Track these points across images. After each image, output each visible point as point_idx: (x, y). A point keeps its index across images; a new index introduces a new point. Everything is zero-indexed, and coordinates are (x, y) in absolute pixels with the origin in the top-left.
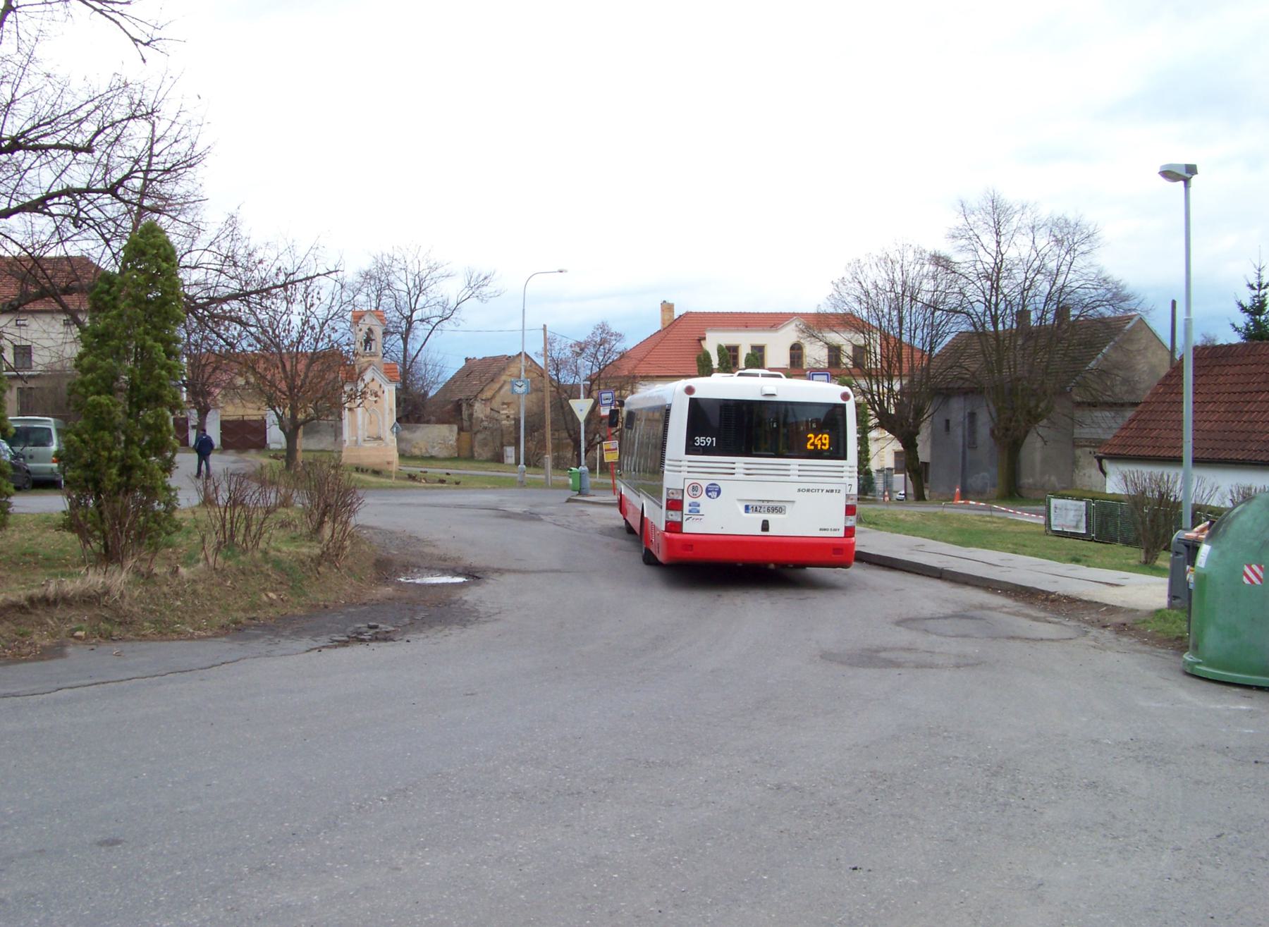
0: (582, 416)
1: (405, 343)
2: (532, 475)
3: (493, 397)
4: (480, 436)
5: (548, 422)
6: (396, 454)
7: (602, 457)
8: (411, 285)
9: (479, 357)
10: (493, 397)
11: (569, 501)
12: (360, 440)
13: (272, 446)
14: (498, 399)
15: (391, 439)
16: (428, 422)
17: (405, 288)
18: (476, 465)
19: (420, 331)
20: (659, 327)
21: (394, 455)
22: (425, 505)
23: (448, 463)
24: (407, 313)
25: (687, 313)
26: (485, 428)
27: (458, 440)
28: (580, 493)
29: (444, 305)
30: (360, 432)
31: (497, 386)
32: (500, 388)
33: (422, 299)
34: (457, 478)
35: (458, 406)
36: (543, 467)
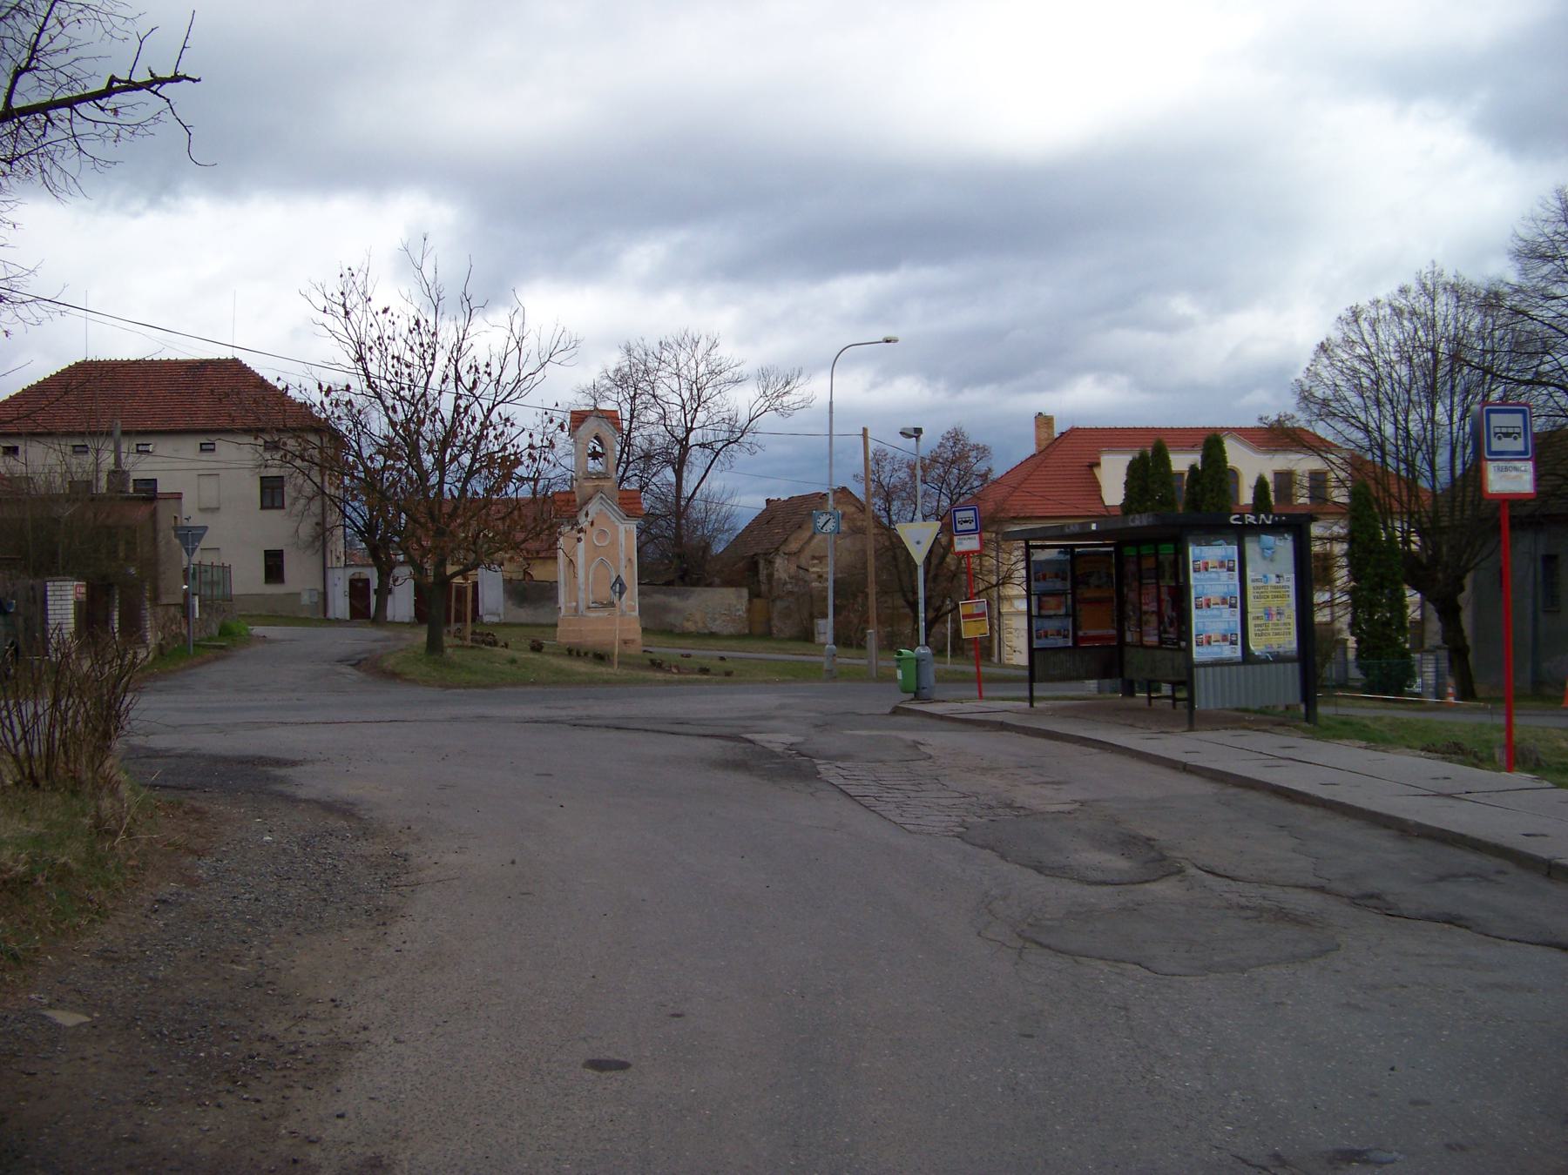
0: (919, 555)
1: (679, 474)
2: (848, 659)
3: (800, 551)
4: (779, 605)
5: (871, 577)
6: (638, 627)
7: (957, 632)
8: (686, 395)
9: (784, 497)
10: (800, 551)
11: (896, 711)
12: (582, 606)
13: (486, 619)
14: (807, 553)
15: (631, 601)
16: (710, 585)
17: (679, 401)
18: (774, 644)
19: (697, 458)
20: (1031, 449)
21: (634, 629)
22: (576, 724)
23: (733, 643)
24: (680, 433)
25: (1073, 430)
26: (791, 593)
27: (749, 611)
28: (918, 696)
29: (731, 422)
30: (582, 595)
31: (807, 534)
32: (811, 538)
33: (701, 416)
34: (728, 665)
35: (753, 566)
36: (861, 646)
